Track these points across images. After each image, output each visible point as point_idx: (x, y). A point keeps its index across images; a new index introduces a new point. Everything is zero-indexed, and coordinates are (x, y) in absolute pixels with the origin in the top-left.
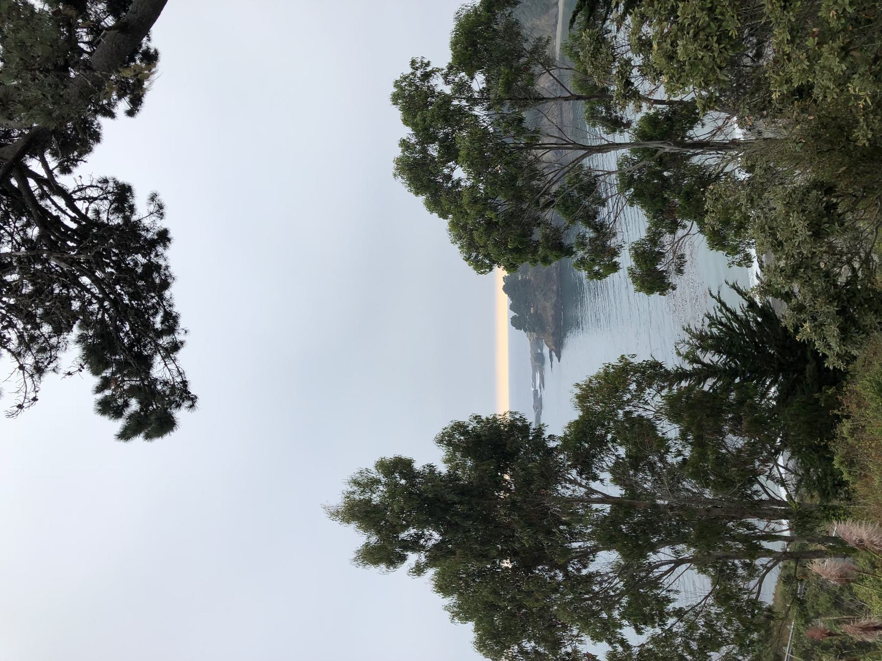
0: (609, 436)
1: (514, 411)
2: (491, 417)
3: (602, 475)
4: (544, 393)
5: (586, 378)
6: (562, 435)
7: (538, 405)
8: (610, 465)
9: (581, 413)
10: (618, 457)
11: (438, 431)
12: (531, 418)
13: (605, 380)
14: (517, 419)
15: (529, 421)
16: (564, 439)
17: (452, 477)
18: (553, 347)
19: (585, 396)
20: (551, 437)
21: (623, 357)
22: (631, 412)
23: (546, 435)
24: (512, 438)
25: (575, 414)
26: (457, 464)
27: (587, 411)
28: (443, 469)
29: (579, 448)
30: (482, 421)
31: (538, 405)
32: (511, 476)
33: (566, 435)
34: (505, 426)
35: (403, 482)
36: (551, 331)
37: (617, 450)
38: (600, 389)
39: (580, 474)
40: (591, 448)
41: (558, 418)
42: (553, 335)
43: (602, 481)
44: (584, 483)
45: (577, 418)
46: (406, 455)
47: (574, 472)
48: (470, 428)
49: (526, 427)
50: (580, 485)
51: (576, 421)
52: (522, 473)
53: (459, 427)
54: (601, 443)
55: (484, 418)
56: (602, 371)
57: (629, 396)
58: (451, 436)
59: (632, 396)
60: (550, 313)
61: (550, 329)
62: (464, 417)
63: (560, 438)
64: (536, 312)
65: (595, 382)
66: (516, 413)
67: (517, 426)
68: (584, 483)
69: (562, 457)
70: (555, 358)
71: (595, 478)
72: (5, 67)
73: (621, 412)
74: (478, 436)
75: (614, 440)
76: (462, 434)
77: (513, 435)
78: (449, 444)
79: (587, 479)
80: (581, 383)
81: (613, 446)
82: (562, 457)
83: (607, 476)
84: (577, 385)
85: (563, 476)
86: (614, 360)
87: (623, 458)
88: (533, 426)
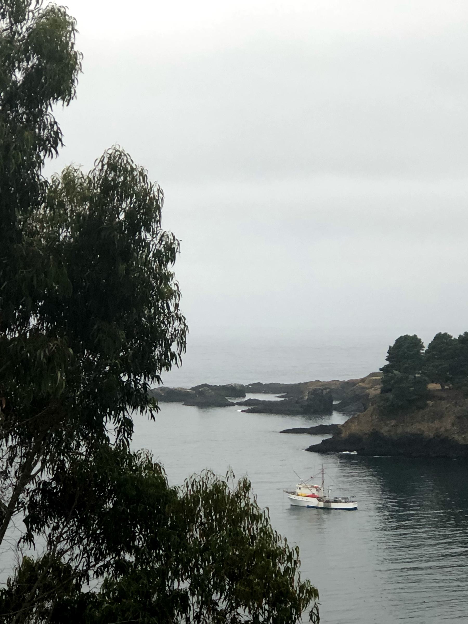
0: (129, 558)
1: (189, 338)
2: (172, 284)
3: (41, 540)
4: (239, 409)
5: (262, 505)
6: (133, 448)
7: (208, 397)
8: (65, 559)
9: (181, 495)
10: (84, 575)
11: (138, 159)
12: (170, 378)
13: (258, 553)
14: (168, 346)
15: (163, 374)
16: (122, 455)
17: (30, 191)
18: (344, 435)
19: (224, 508)
20: (127, 426)
21: (313, 593)
22: (185, 608)
23: (137, 417)
24: (122, 335)
25: (178, 477)
26: (61, 205)
27: (184, 510)
28: (51, 170)
29: (102, 488)
30: (162, 263)
31: (208, 397)
32: (35, 331)
33: (131, 457)
34: (150, 319)
35: (19, 76)
36: (384, 430)
37: (98, 573)
38: (237, 539)
39: (44, 488)
40: (103, 515)
41: (172, 444)
42: (375, 435)
43: (29, 538)
44: (24, 498)
45: (171, 483)
46: (82, 82)
47: (46, 476)
48: (146, 236)
49: (150, 370)
50: (18, 489)
51: (163, 483)
52: (41, 355)
53: (148, 210)
54: (114, 536)
55: (170, 268)
56: (281, 544)
57: (222, 605)
58: (126, 190)
59: (223, 613)
60: (425, 427)
61: (387, 429)
62: (170, 221)
63: (126, 446)
64: (431, 396)
65: (256, 527)
66: (182, 344)
67: (151, 346)
68: (24, 498)
69: (83, 450)
70: (317, 440)
71: (34, 522)
72: (2, 108)
73: (185, 585)
74: (127, 254)
75: (121, 566)
76: (130, 215)
77: (129, 337)
78: (107, 187)
79: (32, 505)
80: (250, 495)
81: (107, 566)
82: (83, 450)
83: (38, 549)
84: (246, 487)
85: (38, 450)
86: (305, 574)
87: (78, 586)
88: (153, 386)
